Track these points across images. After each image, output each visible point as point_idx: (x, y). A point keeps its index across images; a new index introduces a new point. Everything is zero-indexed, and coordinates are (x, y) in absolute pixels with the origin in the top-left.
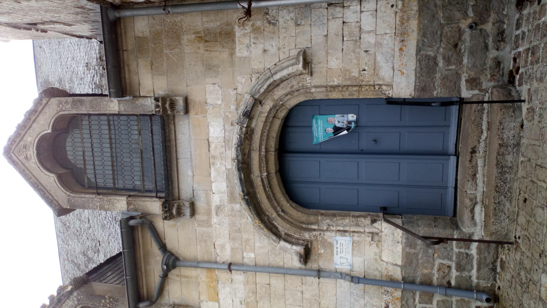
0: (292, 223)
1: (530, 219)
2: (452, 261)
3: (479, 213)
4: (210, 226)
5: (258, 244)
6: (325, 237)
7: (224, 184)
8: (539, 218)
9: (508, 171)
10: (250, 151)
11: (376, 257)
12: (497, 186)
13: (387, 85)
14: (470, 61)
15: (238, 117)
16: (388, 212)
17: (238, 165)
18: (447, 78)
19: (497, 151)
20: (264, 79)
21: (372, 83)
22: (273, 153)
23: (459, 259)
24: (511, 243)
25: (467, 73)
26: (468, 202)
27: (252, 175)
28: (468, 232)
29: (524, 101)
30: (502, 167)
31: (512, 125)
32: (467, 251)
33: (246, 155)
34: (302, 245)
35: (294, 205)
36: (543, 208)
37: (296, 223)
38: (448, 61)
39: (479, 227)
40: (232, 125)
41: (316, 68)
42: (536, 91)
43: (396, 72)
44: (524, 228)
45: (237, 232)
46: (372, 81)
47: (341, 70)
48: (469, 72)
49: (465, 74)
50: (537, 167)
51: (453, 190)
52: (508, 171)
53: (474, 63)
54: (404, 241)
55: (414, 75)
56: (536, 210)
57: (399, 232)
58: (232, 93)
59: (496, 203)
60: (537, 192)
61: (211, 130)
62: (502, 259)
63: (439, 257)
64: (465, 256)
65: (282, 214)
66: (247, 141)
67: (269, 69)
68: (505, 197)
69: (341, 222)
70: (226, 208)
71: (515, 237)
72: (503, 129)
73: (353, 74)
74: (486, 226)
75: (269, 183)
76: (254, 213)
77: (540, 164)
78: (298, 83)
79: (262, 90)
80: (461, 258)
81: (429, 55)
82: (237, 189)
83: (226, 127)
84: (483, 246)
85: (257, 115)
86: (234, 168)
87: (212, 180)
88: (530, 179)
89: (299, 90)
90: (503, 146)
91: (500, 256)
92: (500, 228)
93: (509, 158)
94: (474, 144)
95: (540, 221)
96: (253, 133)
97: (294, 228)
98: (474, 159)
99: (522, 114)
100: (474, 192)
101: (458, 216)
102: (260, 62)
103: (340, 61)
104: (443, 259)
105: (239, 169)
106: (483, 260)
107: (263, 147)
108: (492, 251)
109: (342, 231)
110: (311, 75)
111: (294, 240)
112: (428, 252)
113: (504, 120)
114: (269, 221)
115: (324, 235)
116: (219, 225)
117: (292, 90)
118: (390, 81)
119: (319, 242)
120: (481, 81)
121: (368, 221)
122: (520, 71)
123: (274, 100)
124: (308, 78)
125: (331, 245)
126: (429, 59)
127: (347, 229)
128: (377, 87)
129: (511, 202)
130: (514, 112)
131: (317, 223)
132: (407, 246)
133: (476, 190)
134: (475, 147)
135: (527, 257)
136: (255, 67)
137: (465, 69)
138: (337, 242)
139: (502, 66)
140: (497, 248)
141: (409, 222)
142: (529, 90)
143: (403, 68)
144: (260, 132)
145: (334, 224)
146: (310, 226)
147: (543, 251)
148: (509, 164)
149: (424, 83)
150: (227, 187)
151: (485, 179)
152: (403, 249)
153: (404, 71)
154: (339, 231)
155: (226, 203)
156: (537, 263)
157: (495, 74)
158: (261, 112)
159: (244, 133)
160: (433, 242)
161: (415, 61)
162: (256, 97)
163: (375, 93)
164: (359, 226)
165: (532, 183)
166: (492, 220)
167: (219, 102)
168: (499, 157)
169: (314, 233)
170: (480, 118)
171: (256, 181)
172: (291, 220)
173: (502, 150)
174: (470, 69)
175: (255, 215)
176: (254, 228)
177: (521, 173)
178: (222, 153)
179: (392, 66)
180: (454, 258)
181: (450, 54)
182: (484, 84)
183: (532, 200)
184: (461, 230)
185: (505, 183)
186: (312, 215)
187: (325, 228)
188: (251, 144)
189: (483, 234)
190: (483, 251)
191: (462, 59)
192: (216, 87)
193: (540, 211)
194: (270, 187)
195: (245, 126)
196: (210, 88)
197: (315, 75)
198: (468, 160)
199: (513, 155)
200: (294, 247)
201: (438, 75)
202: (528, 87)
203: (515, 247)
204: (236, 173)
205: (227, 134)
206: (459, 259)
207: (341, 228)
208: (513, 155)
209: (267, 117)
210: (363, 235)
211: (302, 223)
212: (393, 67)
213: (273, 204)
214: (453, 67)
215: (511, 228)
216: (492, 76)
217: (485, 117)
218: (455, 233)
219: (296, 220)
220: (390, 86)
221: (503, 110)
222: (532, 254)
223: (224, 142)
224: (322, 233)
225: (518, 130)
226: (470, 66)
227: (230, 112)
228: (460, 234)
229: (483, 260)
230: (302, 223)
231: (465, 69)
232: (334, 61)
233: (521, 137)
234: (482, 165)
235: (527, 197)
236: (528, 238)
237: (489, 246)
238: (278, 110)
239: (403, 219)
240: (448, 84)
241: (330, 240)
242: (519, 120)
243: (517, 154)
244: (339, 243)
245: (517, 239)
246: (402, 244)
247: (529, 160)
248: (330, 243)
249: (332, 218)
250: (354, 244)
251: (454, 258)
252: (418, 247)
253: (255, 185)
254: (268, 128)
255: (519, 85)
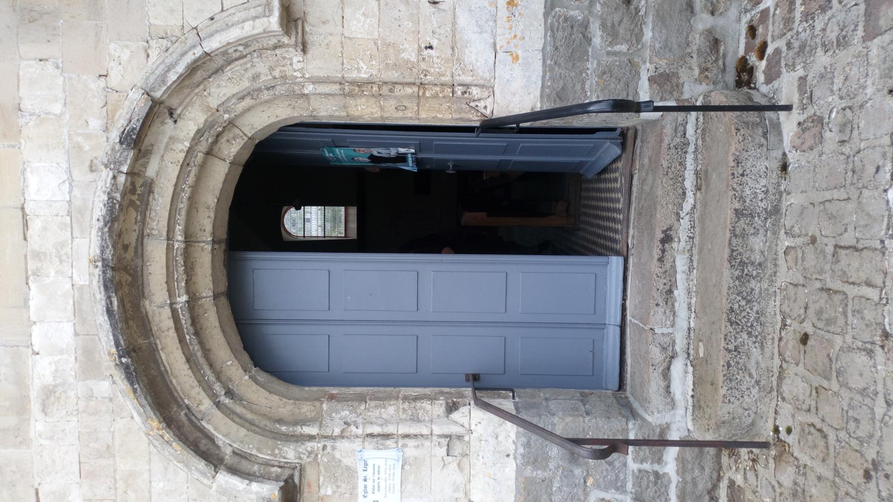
0: (252, 423)
1: (825, 384)
2: (625, 492)
3: (682, 379)
4: (25, 442)
5: (161, 485)
6: (337, 455)
7: (68, 329)
8: (857, 377)
9: (754, 273)
10: (141, 237)
11: (457, 495)
12: (732, 310)
13: (482, 86)
14: (657, 35)
15: (108, 149)
16: (482, 385)
17: (104, 272)
18: (610, 71)
19: (729, 227)
20: (179, 51)
21: (447, 79)
22: (209, 247)
23: (640, 487)
24: (765, 445)
25: (651, 63)
26: (656, 354)
27: (147, 303)
28: (659, 422)
29: (788, 108)
30: (743, 264)
31: (762, 165)
32: (656, 467)
33: (131, 250)
34: (277, 479)
35: (263, 377)
36: (870, 353)
37: (264, 423)
38: (612, 33)
39: (680, 411)
40: (92, 169)
41: (316, 33)
42: (826, 76)
43: (500, 55)
44: (805, 407)
45: (101, 456)
46: (448, 74)
47: (375, 44)
48: (656, 59)
49: (648, 65)
50: (843, 252)
51: (618, 329)
52: (754, 273)
53: (667, 40)
54: (521, 450)
55: (540, 63)
56: (845, 359)
57: (510, 429)
58: (93, 86)
59: (729, 351)
60: (845, 314)
61: (33, 181)
62: (732, 483)
63: (597, 485)
64: (652, 478)
65: (227, 401)
66: (133, 214)
67: (196, 28)
68: (749, 334)
69: (377, 413)
70: (72, 394)
71: (776, 430)
72: (742, 175)
73: (405, 55)
74: (698, 405)
75: (194, 321)
76: (144, 402)
77: (853, 242)
78: (271, 69)
79: (172, 77)
80: (644, 483)
81: (573, 19)
82: (104, 340)
83: (76, 175)
84: (689, 452)
85: (162, 146)
86: (95, 282)
87: (33, 318)
88: (818, 285)
89: (273, 87)
90: (743, 215)
91: (728, 475)
92: (740, 411)
93: (757, 243)
94: (669, 222)
95: (861, 385)
96: (151, 191)
97: (258, 437)
98: (668, 255)
99: (781, 141)
100: (670, 330)
101: (628, 388)
102: (172, 11)
103: (375, 21)
104: (606, 489)
105: (107, 286)
106: (689, 487)
107: (179, 229)
108: (709, 465)
109: (379, 435)
110: (304, 51)
111: (256, 468)
112: (574, 476)
113: (746, 155)
114: (190, 420)
115: (334, 448)
116: (51, 438)
117: (257, 85)
118: (487, 75)
119: (322, 468)
120: (681, 81)
121: (438, 408)
122: (769, 50)
123: (209, 108)
124: (296, 57)
125: (351, 472)
126: (572, 27)
127: (390, 429)
128: (459, 90)
129: (762, 347)
130: (765, 135)
131: (316, 419)
132: (528, 463)
133: (673, 326)
134: (670, 229)
135: (819, 478)
136: (158, 22)
137: (647, 53)
138: (366, 464)
139: (722, 48)
140: (718, 456)
141: (529, 407)
142: (803, 80)
143: (516, 46)
144: (171, 190)
145: (360, 420)
146: (299, 430)
147: (875, 465)
148: (757, 258)
149: (562, 82)
150: (76, 334)
151: (693, 301)
152: (519, 472)
153: (520, 52)
154: (371, 435)
155: (71, 380)
156: (853, 492)
157: (709, 66)
158: (172, 139)
159: (121, 188)
160: (595, 451)
161: (542, 28)
162: (158, 94)
163: (455, 107)
164: (419, 421)
165: (825, 295)
166: (723, 391)
167: (57, 108)
168: (734, 241)
169: (310, 445)
170: (681, 164)
171: (157, 319)
172: (249, 416)
173: (742, 223)
174: (657, 54)
175: (148, 408)
176: (150, 443)
177: (784, 276)
178: (63, 245)
179: (492, 41)
180: (629, 486)
181: (617, 19)
182: (686, 87)
183: (828, 336)
184: (643, 420)
185: (748, 302)
186: (306, 399)
187: (337, 431)
188: (144, 221)
189: (691, 428)
190: (690, 466)
191: (641, 29)
192: (49, 67)
193: (861, 359)
194: (197, 333)
195: (125, 169)
196: (30, 69)
197: (312, 51)
198: (656, 257)
199: (765, 236)
200: (255, 486)
201: (591, 65)
202: (801, 72)
203: (773, 453)
204: (100, 296)
205: (76, 192)
206: (640, 487)
207: (376, 430)
208: (765, 236)
209: (190, 151)
210: (427, 443)
211: (280, 421)
212: (495, 44)
213: (203, 376)
214: (623, 48)
215: (764, 408)
216: (704, 70)
217: (690, 158)
218: (630, 426)
219: (264, 416)
220: (488, 87)
221: (742, 132)
222: (837, 472)
223: (69, 214)
224: (329, 444)
225: (774, 176)
226: (657, 46)
227: (88, 136)
228: (641, 427)
229: (689, 487)
230: (280, 421)
231: (647, 53)
232: (359, 21)
233: (781, 194)
234: (686, 268)
235: (810, 330)
236: (820, 430)
237: (701, 455)
238: (219, 135)
239: (517, 399)
240: (612, 86)
241: (347, 461)
242: (778, 154)
243: (774, 233)
244: (370, 468)
245: (783, 435)
246: (515, 458)
247: (813, 240)
248: (348, 468)
249: (356, 404)
250: (407, 467)
251: (629, 486)
252: (552, 465)
253: (155, 329)
254: (191, 180)
255: (768, 81)
